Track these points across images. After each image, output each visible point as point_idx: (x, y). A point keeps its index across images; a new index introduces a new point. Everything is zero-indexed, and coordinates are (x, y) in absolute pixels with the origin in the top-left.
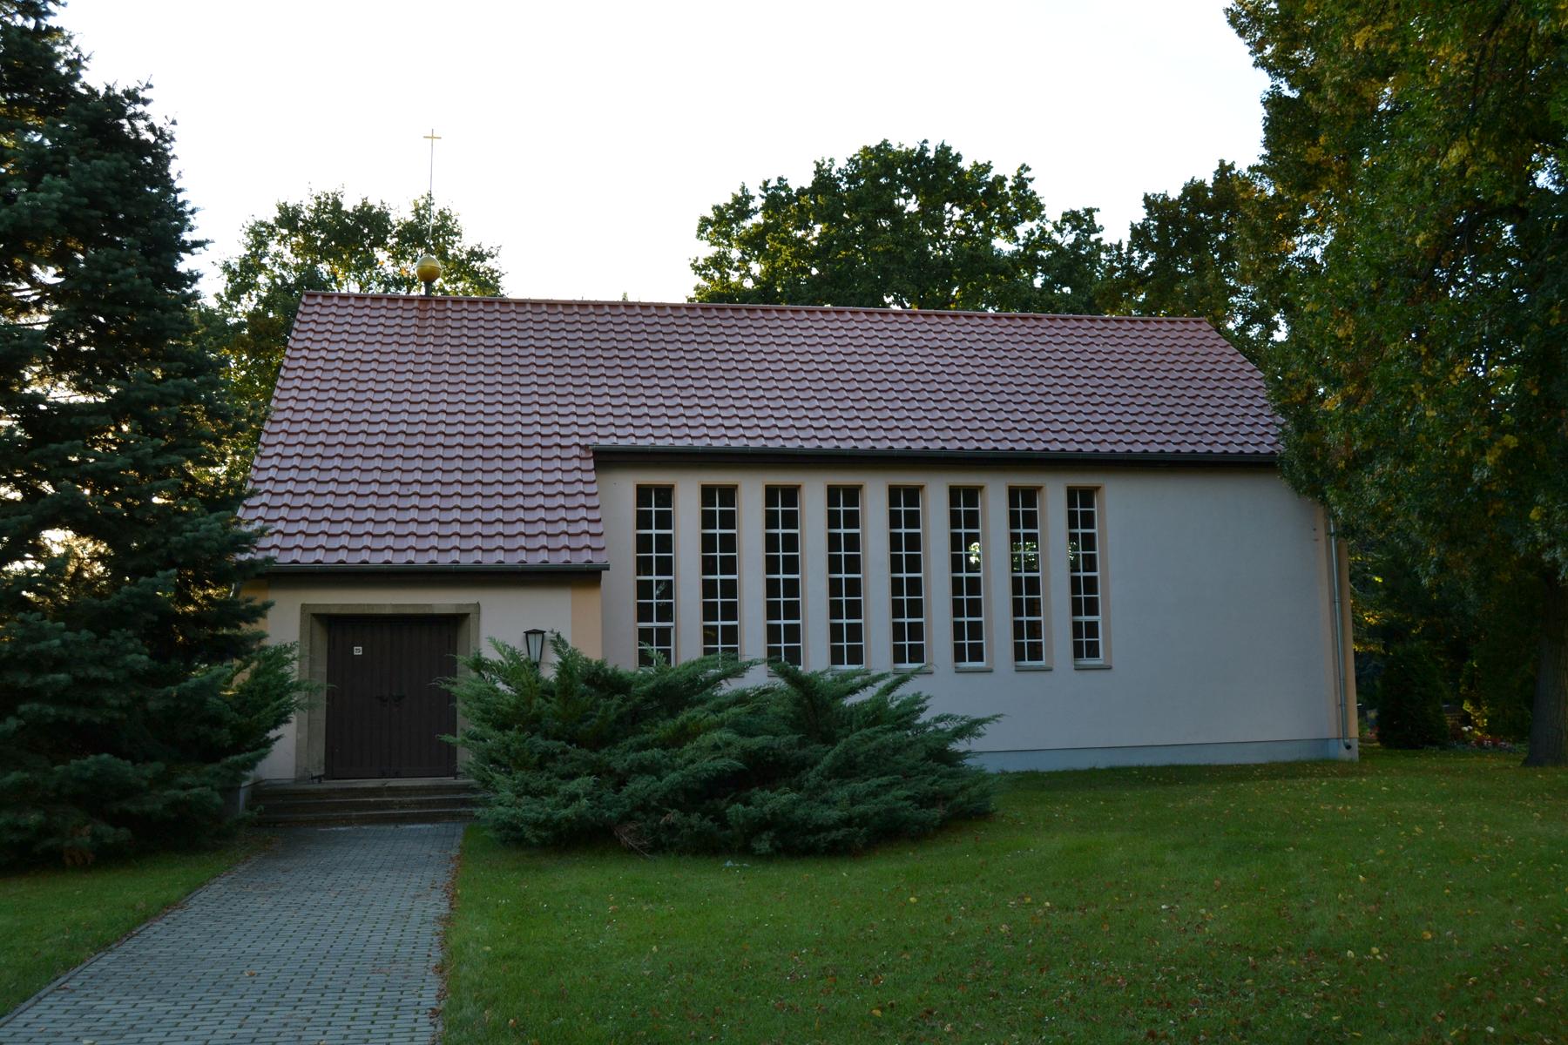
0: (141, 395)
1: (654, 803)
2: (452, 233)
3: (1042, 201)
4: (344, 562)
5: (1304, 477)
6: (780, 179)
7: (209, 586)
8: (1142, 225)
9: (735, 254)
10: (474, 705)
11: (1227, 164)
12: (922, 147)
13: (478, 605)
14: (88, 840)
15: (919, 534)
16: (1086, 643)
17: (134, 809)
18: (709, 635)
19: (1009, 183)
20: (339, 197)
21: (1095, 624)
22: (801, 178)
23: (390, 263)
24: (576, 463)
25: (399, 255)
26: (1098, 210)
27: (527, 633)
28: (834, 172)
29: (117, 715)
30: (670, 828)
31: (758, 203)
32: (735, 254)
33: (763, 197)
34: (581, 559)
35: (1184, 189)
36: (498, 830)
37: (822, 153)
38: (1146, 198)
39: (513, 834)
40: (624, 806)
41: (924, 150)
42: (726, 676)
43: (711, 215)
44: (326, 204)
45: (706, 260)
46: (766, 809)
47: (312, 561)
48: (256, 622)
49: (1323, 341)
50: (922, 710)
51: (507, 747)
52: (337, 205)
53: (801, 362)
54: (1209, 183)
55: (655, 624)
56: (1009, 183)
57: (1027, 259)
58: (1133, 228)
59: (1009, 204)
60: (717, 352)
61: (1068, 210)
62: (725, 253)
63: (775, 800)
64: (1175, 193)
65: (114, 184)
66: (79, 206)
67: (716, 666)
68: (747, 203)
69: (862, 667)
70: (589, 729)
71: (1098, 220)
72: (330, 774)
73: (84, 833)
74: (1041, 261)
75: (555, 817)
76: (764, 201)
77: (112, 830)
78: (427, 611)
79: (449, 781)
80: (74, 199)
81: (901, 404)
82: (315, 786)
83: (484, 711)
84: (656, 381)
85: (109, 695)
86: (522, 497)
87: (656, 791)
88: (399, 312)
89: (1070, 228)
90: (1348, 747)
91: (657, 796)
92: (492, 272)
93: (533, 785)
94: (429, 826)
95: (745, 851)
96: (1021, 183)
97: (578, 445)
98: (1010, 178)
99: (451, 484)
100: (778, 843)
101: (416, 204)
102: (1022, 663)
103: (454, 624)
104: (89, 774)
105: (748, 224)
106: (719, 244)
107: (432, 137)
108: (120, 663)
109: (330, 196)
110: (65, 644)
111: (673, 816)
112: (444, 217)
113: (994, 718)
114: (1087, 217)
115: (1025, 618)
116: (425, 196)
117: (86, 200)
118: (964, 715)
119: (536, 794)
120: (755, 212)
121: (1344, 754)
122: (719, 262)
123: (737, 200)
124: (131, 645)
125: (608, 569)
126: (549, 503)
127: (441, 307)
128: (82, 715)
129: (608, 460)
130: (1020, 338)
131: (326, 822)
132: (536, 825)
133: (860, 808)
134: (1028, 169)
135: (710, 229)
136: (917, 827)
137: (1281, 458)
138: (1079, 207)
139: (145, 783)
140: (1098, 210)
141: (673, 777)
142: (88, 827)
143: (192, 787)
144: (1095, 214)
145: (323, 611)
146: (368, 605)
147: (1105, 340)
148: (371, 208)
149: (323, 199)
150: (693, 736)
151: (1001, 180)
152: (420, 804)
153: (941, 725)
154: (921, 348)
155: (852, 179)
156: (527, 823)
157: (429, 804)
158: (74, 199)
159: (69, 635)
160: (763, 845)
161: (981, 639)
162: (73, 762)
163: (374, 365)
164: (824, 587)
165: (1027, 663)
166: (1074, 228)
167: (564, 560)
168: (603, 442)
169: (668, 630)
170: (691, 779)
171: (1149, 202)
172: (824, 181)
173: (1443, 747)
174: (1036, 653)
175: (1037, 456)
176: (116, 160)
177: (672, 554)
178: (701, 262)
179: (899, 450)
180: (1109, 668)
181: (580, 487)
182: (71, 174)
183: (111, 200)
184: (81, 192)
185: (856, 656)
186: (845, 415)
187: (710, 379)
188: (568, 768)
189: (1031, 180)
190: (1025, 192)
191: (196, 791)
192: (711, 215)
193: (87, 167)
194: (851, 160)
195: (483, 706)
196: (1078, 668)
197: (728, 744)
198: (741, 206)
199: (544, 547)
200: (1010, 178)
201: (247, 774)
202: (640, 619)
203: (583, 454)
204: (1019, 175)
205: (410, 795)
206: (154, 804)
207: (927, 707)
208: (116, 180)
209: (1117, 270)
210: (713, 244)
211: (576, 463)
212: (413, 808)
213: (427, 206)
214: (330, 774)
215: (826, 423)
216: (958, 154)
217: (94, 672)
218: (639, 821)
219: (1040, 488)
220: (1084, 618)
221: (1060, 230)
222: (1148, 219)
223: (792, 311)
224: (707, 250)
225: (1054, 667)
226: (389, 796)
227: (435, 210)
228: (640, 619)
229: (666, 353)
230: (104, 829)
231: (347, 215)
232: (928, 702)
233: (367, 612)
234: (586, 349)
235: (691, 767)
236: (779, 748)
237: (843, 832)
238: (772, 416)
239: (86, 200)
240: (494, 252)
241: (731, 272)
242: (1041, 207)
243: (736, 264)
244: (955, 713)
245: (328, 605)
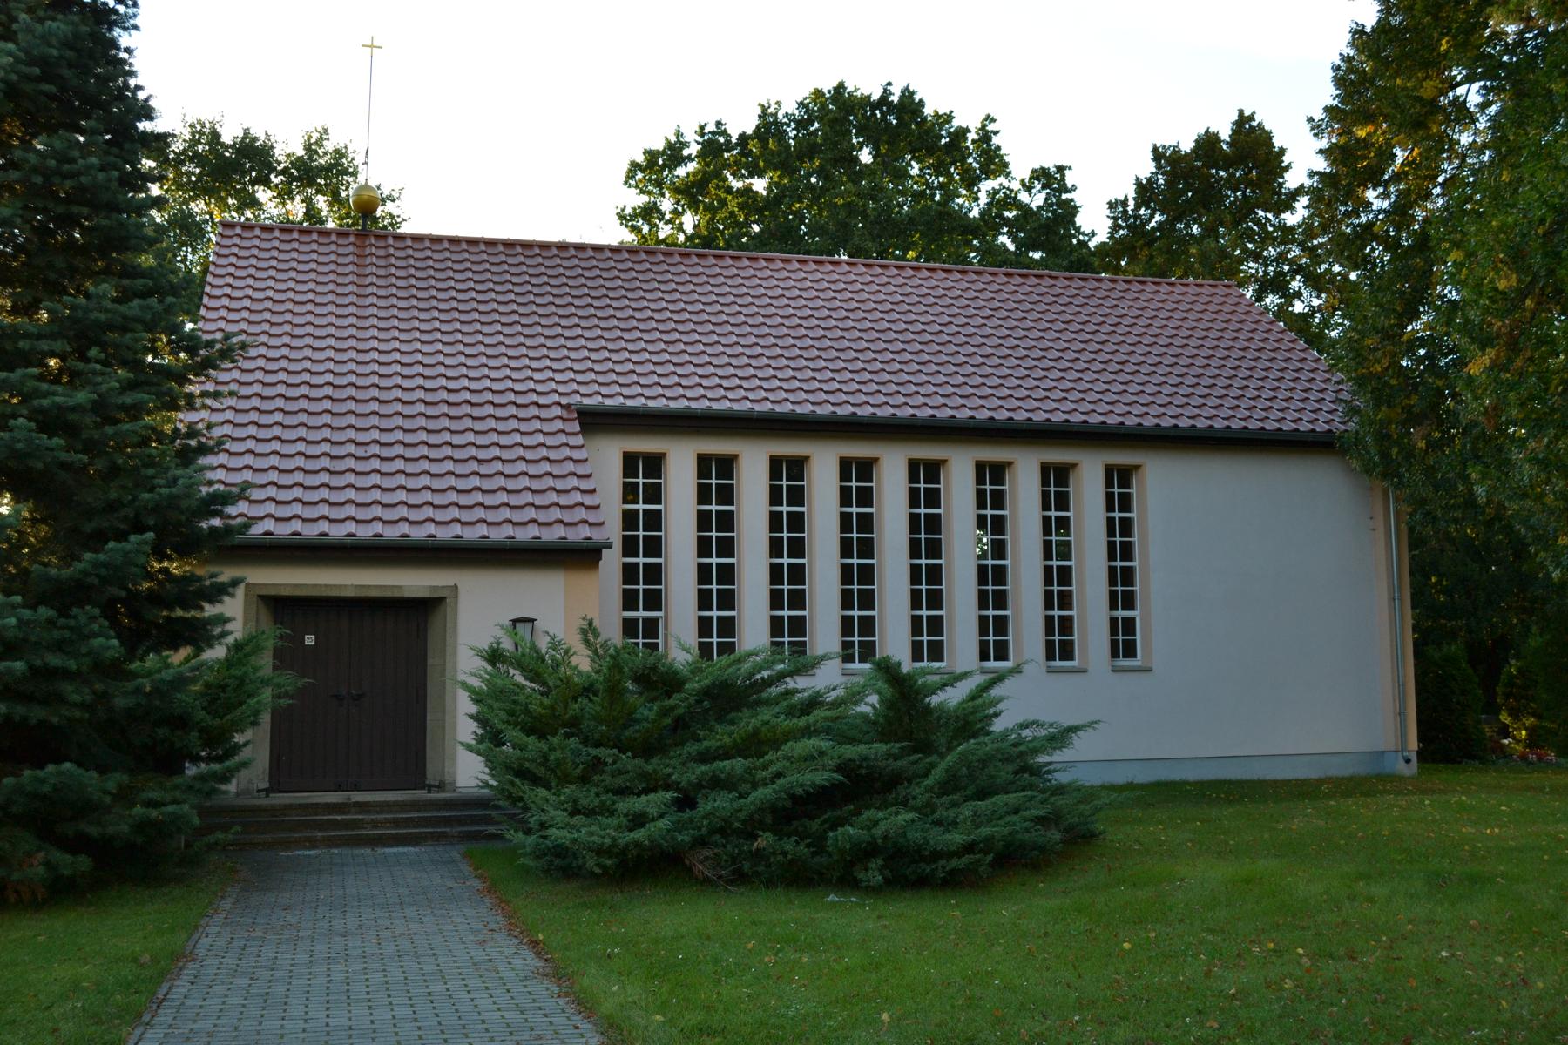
0: (102, 317)
1: (737, 825)
2: (345, 172)
3: (1006, 158)
4: (299, 534)
5: (1376, 459)
6: (718, 124)
7: (170, 559)
8: (1149, 180)
9: (667, 205)
10: (496, 705)
11: (1247, 114)
12: (885, 90)
13: (456, 586)
14: (41, 870)
15: (939, 515)
16: (1123, 642)
17: (94, 831)
18: (776, 626)
19: (972, 136)
20: (217, 127)
21: (1133, 620)
22: (742, 122)
23: (273, 204)
24: (559, 425)
25: (284, 195)
26: (1070, 168)
27: (515, 622)
28: (780, 116)
29: (78, 714)
30: (758, 855)
31: (693, 149)
32: (667, 205)
33: (698, 143)
34: (579, 534)
35: (1196, 141)
36: (538, 857)
37: (768, 96)
38: (1155, 150)
39: (557, 862)
40: (699, 829)
41: (886, 93)
42: (791, 674)
43: (640, 159)
44: (201, 133)
45: (634, 209)
46: (877, 832)
47: (289, 532)
48: (221, 602)
49: (1481, 293)
50: (996, 715)
51: (545, 757)
52: (215, 135)
53: (646, 342)
54: (1225, 134)
55: (642, 613)
56: (972, 136)
57: (991, 220)
58: (1138, 183)
59: (970, 160)
60: (563, 327)
61: (1037, 167)
62: (655, 203)
63: (892, 821)
64: (1187, 146)
65: (70, 54)
66: (28, 78)
67: (783, 662)
68: (681, 149)
69: (942, 664)
70: (638, 735)
71: (1070, 179)
72: (275, 786)
73: (36, 863)
74: (1007, 222)
75: (622, 842)
76: (699, 147)
77: (68, 858)
78: (397, 594)
79: (421, 794)
80: (24, 69)
81: (830, 375)
82: (263, 801)
83: (511, 713)
84: (524, 350)
85: (70, 688)
86: (500, 463)
87: (741, 810)
88: (333, 247)
89: (1039, 187)
90: (1408, 761)
91: (742, 815)
92: (392, 217)
93: (584, 802)
94: (417, 849)
95: (847, 881)
96: (985, 136)
97: (558, 404)
98: (973, 130)
99: (318, 457)
100: (888, 873)
101: (310, 138)
102: (1052, 663)
103: (427, 608)
104: (46, 789)
105: (681, 171)
106: (650, 193)
107: (372, 46)
108: (84, 650)
109: (207, 125)
110: (21, 622)
111: (764, 841)
112: (339, 154)
113: (1091, 724)
114: (1058, 176)
115: (1056, 613)
116: (320, 129)
117: (37, 71)
118: (1052, 721)
119: (590, 813)
120: (689, 158)
121: (1402, 768)
122: (649, 212)
123: (670, 146)
124: (95, 627)
125: (610, 547)
126: (412, 483)
127: (382, 244)
128: (37, 713)
129: (595, 421)
130: (888, 325)
131: (287, 845)
132: (599, 851)
133: (986, 831)
134: (993, 120)
135: (640, 175)
136: (1036, 852)
137: (1340, 437)
138: (1050, 164)
139: (108, 800)
140: (1070, 168)
141: (763, 793)
142: (42, 854)
143: (164, 804)
144: (1067, 172)
145: (272, 592)
146: (326, 586)
147: (1131, 303)
148: (255, 139)
149: (199, 128)
150: (776, 744)
151: (962, 133)
152: (397, 823)
153: (1026, 733)
154: (763, 336)
155: (801, 124)
156: (590, 849)
157: (408, 822)
158: (24, 69)
159: (26, 614)
160: (873, 874)
161: (1072, 635)
162: (27, 773)
163: (310, 307)
164: (835, 575)
165: (1058, 663)
166: (1044, 187)
167: (583, 536)
168: (586, 401)
169: (655, 621)
170: (783, 795)
171: (1158, 154)
172: (769, 126)
173: (1483, 760)
174: (1067, 652)
175: (1075, 429)
176: (73, 23)
177: (662, 533)
178: (628, 211)
179: (923, 419)
180: (1085, 671)
181: (567, 452)
182: (20, 36)
183: (66, 73)
184: (31, 62)
185: (936, 652)
186: (751, 396)
187: (610, 351)
188: (619, 781)
189: (996, 133)
190: (989, 145)
191: (170, 808)
192: (640, 159)
193: (39, 28)
194: (801, 104)
195: (508, 705)
196: (1115, 670)
197: (822, 753)
198: (674, 153)
199: (534, 521)
200: (973, 130)
201: (223, 787)
202: (625, 608)
203: (565, 414)
204: (983, 127)
205: (381, 812)
206: (119, 825)
207: (1001, 712)
208: (71, 49)
209: (1121, 227)
210: (642, 192)
211: (559, 425)
212: (388, 828)
213: (319, 143)
214: (275, 786)
215: (743, 393)
216: (921, 101)
217: (54, 660)
218: (716, 845)
219: (1074, 466)
220: (1121, 614)
221: (1028, 189)
222: (1157, 173)
223: (765, 259)
224: (634, 199)
225: (1090, 669)
226: (357, 813)
227: (329, 146)
228: (625, 608)
229: (537, 319)
230: (58, 856)
231: (226, 147)
232: (1000, 706)
233: (324, 594)
234: (400, 330)
235: (781, 781)
236: (876, 759)
237: (966, 859)
238: (721, 386)
239: (37, 71)
240: (395, 195)
241: (661, 225)
242: (1006, 165)
243: (668, 217)
244: (1041, 718)
245: (320, 586)
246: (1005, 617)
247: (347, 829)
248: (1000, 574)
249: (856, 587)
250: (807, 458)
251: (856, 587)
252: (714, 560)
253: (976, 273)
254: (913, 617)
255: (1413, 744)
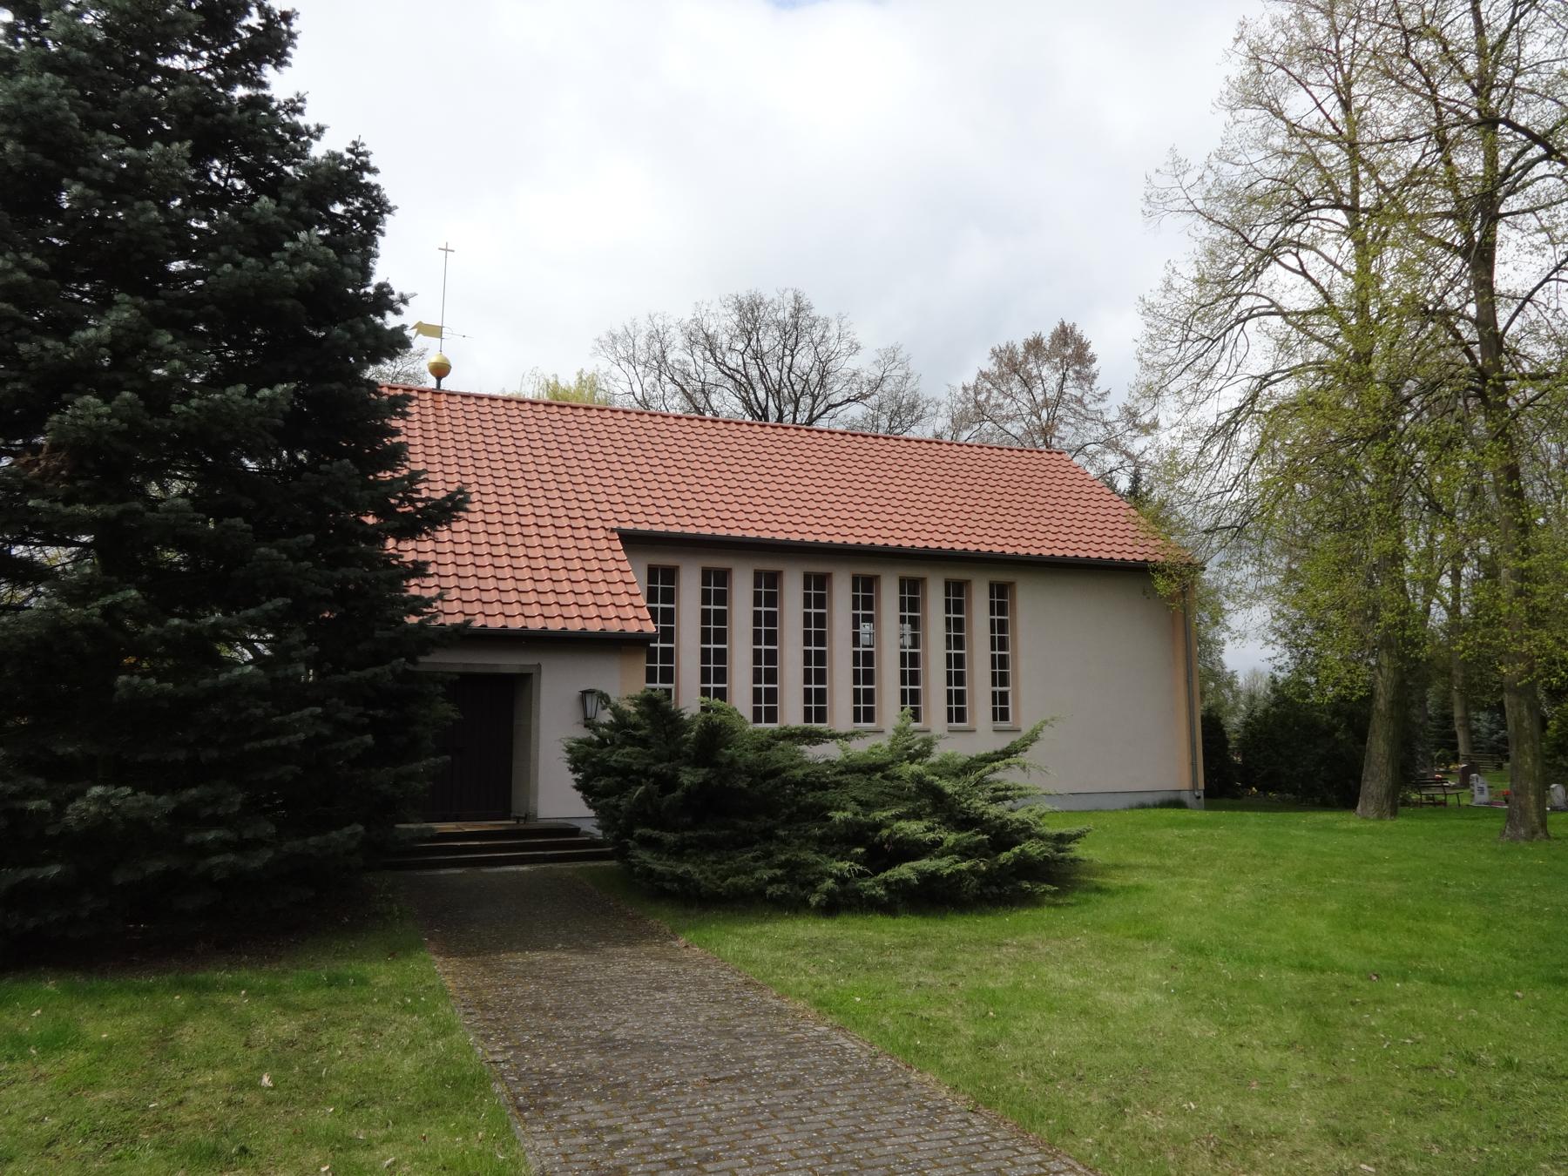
78: (495, 670)
107: (446, 250)
165: (954, 724)
220: (998, 689)
225: (979, 730)
246: (824, 690)
247: (513, 839)
248: (915, 659)
249: (712, 666)
250: (730, 570)
251: (712, 666)
252: (712, 646)
253: (772, 427)
254: (755, 689)
255: (1202, 785)
